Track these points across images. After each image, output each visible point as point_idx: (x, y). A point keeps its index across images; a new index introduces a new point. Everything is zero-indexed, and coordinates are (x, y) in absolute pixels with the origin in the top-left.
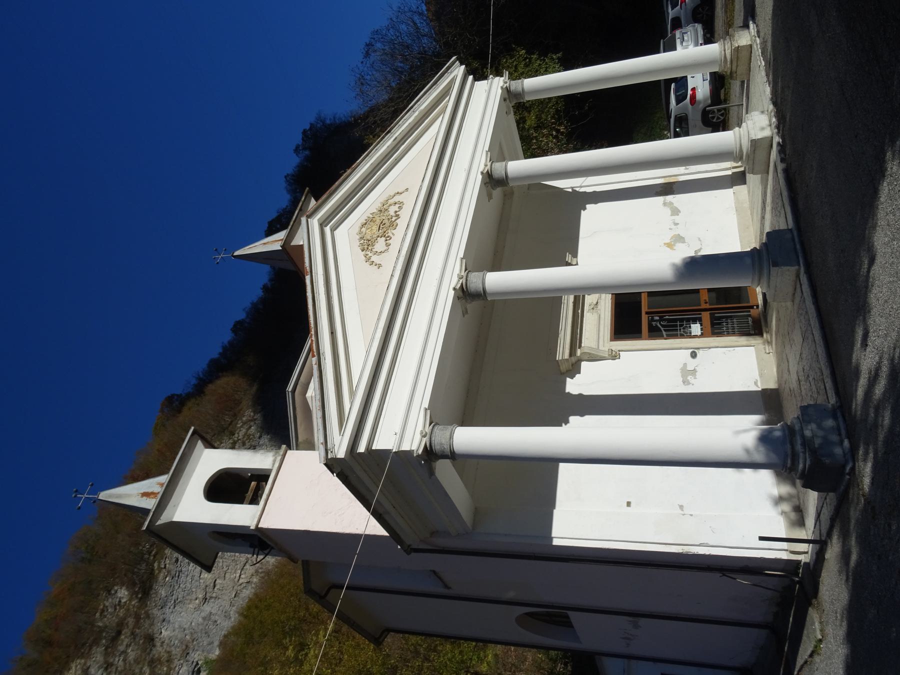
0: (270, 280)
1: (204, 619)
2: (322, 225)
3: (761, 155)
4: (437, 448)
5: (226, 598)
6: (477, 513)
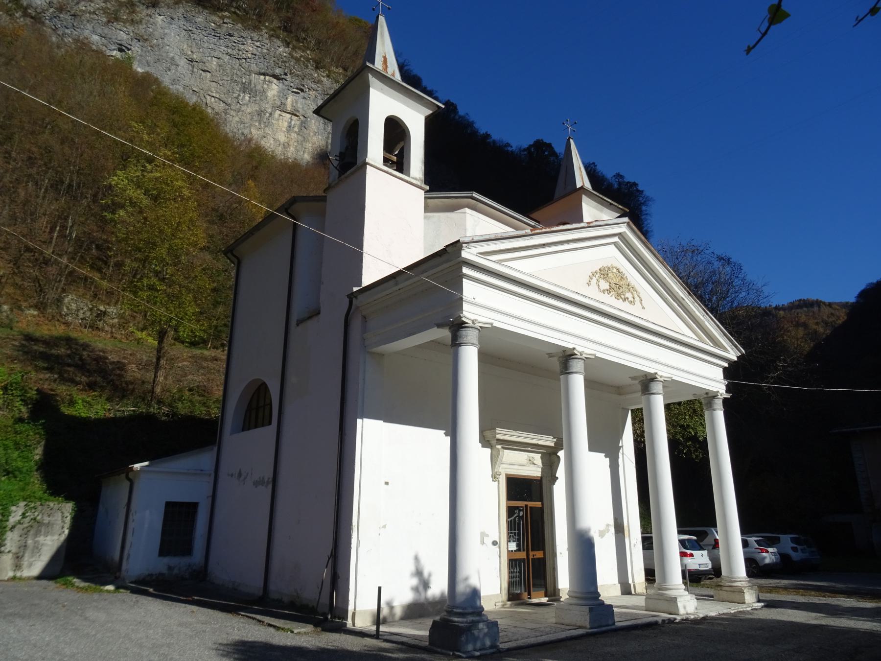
0: (494, 141)
1: (173, 59)
2: (620, 235)
3: (664, 605)
4: (464, 332)
5: (192, 82)
6: (381, 355)
